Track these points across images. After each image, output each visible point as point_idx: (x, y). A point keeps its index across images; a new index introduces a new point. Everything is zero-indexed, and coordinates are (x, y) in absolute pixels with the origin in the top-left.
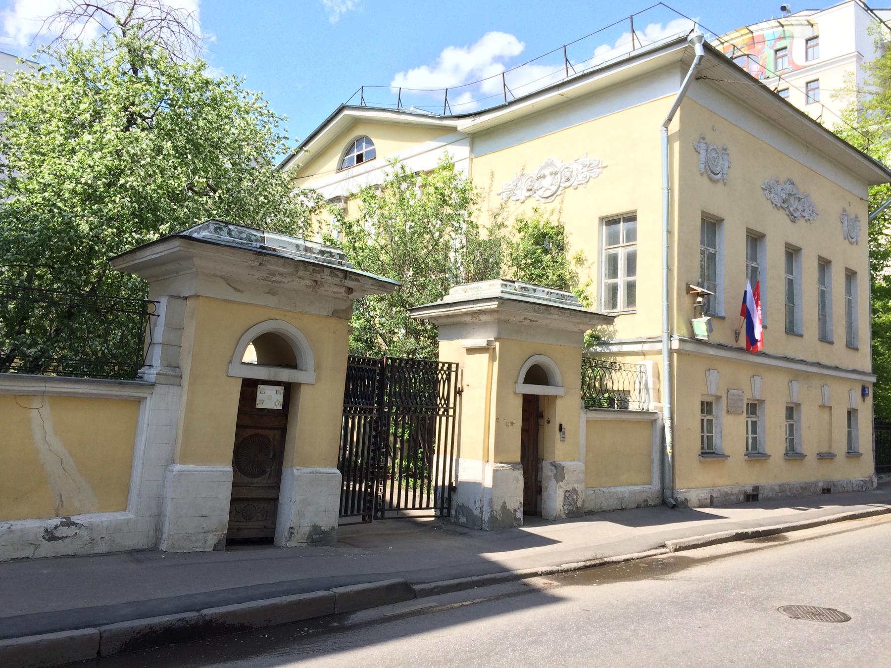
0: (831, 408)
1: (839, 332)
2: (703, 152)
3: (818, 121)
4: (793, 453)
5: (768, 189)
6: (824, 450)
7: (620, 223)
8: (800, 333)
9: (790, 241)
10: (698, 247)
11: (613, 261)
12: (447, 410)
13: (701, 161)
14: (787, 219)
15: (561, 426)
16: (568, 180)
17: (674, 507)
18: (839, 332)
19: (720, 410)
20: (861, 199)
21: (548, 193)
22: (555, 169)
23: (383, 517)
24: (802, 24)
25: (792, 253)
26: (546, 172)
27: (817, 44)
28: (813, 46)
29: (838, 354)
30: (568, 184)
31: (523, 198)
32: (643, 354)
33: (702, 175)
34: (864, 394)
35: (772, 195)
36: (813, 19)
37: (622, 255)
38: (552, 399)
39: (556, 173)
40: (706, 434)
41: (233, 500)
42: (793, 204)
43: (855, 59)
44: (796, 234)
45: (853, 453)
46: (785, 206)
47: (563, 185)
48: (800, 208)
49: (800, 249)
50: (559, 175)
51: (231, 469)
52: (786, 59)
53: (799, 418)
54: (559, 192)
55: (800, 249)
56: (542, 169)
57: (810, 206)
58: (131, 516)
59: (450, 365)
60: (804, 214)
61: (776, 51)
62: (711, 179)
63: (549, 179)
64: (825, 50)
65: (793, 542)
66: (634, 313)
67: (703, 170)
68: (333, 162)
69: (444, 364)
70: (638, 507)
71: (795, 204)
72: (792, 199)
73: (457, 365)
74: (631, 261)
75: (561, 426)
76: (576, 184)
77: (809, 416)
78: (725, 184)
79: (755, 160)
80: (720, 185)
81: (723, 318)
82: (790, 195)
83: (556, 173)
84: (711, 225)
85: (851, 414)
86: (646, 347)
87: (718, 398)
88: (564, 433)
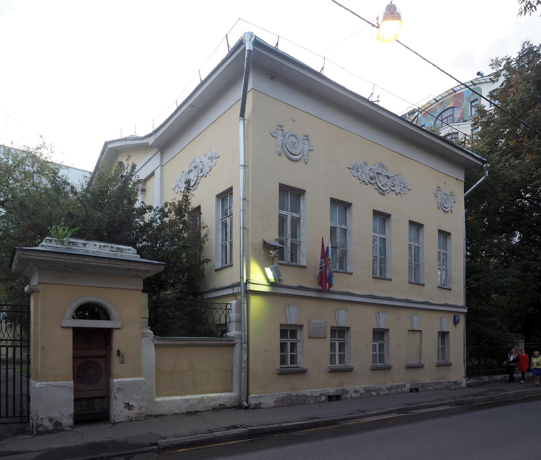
0: (421, 331)
2: (280, 138)
3: (370, 100)
4: (380, 366)
6: (413, 362)
8: (422, 282)
10: (275, 212)
14: (376, 193)
15: (118, 351)
17: (246, 408)
19: (302, 337)
24: (487, 82)
29: (430, 293)
30: (202, 174)
33: (280, 155)
35: (359, 173)
38: (108, 333)
41: (76, 400)
42: (379, 181)
44: (383, 204)
45: (444, 364)
48: (389, 184)
49: (391, 215)
51: (72, 382)
53: (388, 338)
55: (391, 215)
56: (189, 167)
61: (471, 102)
70: (213, 409)
75: (118, 351)
78: (306, 163)
80: (301, 164)
81: (305, 267)
85: (443, 335)
87: (301, 327)
88: (123, 357)
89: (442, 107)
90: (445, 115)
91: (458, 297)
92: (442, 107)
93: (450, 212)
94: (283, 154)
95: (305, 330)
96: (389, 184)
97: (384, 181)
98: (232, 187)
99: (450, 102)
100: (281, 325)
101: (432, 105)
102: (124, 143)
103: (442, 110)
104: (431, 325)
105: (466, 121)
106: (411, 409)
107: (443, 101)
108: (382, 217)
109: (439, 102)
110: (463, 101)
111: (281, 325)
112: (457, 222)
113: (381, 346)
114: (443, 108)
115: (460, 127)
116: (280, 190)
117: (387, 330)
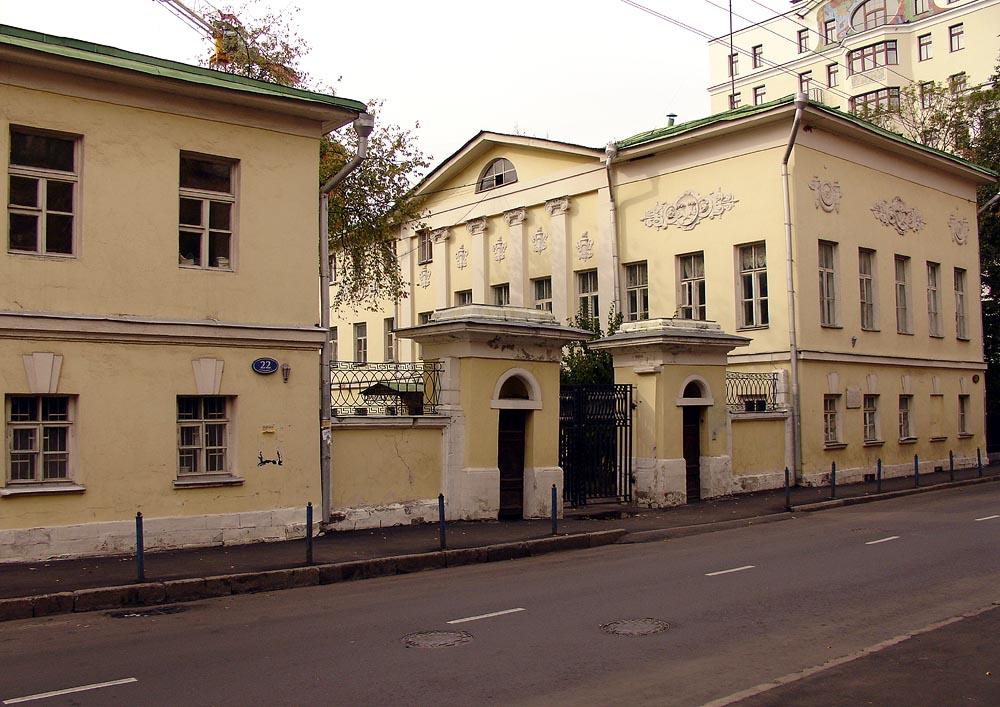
0: (942, 396)
1: (949, 328)
5: (878, 209)
7: (749, 251)
8: (967, 338)
10: (818, 269)
12: (625, 421)
16: (705, 211)
19: (840, 406)
21: (688, 222)
22: (694, 200)
23: (585, 504)
25: (901, 260)
26: (685, 202)
28: (927, 44)
29: (951, 353)
30: (705, 215)
34: (975, 380)
46: (893, 221)
59: (626, 386)
63: (688, 210)
65: (397, 314)
66: (767, 328)
68: (474, 178)
69: (621, 386)
73: (631, 385)
77: (920, 408)
80: (834, 213)
84: (827, 247)
85: (963, 398)
91: (975, 353)
95: (843, 398)
96: (908, 221)
97: (902, 217)
104: (950, 386)
105: (908, 22)
106: (948, 479)
108: (901, 260)
112: (969, 256)
113: (906, 414)
115: (899, 31)
116: (819, 244)
117: (233, 398)
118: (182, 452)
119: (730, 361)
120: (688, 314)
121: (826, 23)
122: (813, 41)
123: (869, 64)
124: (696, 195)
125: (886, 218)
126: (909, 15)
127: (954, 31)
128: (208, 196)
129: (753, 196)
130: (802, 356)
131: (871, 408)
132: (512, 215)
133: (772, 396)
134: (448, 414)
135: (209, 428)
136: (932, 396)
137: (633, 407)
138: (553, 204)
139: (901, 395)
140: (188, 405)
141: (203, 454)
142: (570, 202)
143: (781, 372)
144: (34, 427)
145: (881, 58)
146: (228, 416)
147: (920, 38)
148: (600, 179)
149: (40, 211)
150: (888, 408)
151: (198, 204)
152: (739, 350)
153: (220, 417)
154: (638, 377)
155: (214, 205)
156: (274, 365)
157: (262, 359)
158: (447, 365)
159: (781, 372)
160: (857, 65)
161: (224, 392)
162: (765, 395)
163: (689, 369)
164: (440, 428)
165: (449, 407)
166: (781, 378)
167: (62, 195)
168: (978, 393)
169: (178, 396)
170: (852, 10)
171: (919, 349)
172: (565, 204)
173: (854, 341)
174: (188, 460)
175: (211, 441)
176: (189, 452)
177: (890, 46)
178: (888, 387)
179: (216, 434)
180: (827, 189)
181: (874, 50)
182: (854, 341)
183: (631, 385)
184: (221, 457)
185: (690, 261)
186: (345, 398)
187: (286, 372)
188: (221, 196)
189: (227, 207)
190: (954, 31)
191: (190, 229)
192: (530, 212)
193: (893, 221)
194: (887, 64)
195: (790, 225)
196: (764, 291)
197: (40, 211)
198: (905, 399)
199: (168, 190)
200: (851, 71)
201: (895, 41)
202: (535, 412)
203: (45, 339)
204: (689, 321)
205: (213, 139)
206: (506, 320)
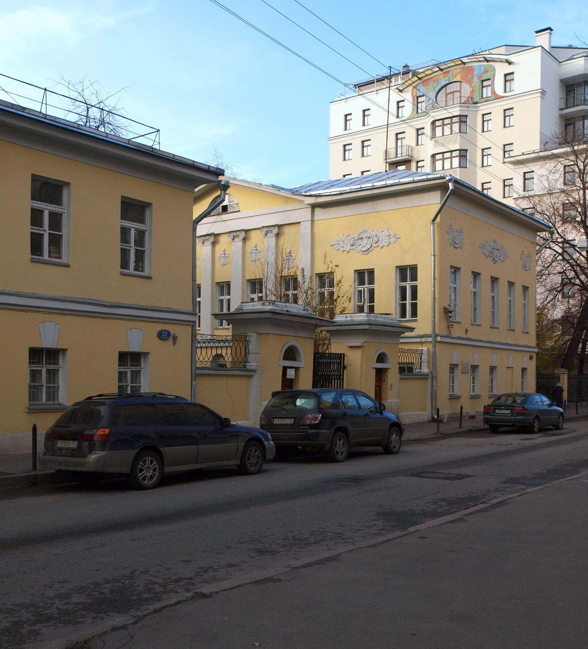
0: (512, 367)
2: (451, 233)
5: (482, 247)
7: (407, 273)
9: (493, 276)
11: (403, 290)
12: (340, 377)
13: (449, 239)
18: (518, 325)
20: (532, 242)
25: (494, 280)
26: (364, 236)
27: (513, 80)
31: (348, 250)
32: (421, 343)
34: (531, 358)
35: (485, 250)
36: (511, 58)
37: (408, 285)
39: (370, 238)
40: (451, 385)
43: (539, 95)
46: (491, 255)
47: (374, 245)
50: (371, 238)
52: (489, 88)
54: (371, 249)
57: (504, 252)
58: (251, 422)
60: (500, 258)
62: (454, 247)
63: (365, 241)
64: (518, 86)
67: (451, 243)
71: (496, 253)
72: (495, 251)
73: (344, 354)
74: (414, 290)
76: (381, 245)
79: (477, 228)
82: (493, 248)
83: (370, 238)
84: (456, 270)
85: (524, 370)
86: (423, 340)
89: (447, 78)
90: (450, 88)
92: (447, 78)
93: (460, 248)
94: (452, 245)
95: (460, 367)
98: (472, 272)
99: (456, 75)
100: (450, 364)
101: (434, 72)
102: (204, 214)
103: (447, 82)
107: (449, 71)
108: (494, 280)
109: (444, 71)
110: (473, 77)
111: (450, 364)
114: (449, 80)
115: (469, 109)
118: (30, 386)
119: (402, 340)
120: (361, 309)
121: (418, 98)
122: (407, 110)
123: (447, 130)
124: (371, 232)
125: (487, 253)
126: (477, 98)
127: (507, 113)
128: (133, 226)
129: (410, 234)
130: (439, 339)
131: (473, 374)
132: (234, 234)
133: (419, 364)
134: (254, 368)
135: (48, 371)
136: (507, 367)
137: (344, 367)
138: (267, 229)
139: (490, 366)
140: (36, 354)
141: (45, 386)
142: (279, 229)
143: (425, 348)
144: (41, 368)
145: (456, 127)
146: (455, 373)
147: (483, 115)
148: (305, 214)
149: (45, 231)
150: (483, 373)
151: (41, 212)
152: (407, 334)
153: (54, 364)
154: (349, 350)
155: (51, 214)
156: (169, 334)
157: (165, 331)
158: (253, 338)
159: (425, 348)
160: (439, 131)
161: (59, 347)
162: (414, 363)
163: (376, 347)
164: (251, 377)
165: (255, 364)
166: (425, 353)
167: (56, 220)
168: (532, 367)
169: (29, 348)
170: (437, 89)
171: (502, 336)
172: (276, 230)
173: (467, 331)
174: (34, 393)
175: (49, 381)
176: (34, 387)
177: (462, 119)
178: (484, 360)
179: (53, 375)
180: (456, 233)
181: (452, 121)
182: (467, 331)
183: (344, 354)
184: (54, 392)
185: (365, 276)
186: (204, 357)
187: (175, 339)
188: (141, 227)
189: (60, 215)
190: (507, 113)
191: (37, 230)
192: (248, 233)
193: (491, 255)
194: (460, 132)
195: (434, 256)
196: (125, 253)
197: (45, 231)
198: (492, 369)
199: (114, 220)
200: (433, 136)
201: (467, 116)
202: (301, 368)
203: (51, 313)
204: (296, 306)
205: (53, 167)
206: (288, 311)
